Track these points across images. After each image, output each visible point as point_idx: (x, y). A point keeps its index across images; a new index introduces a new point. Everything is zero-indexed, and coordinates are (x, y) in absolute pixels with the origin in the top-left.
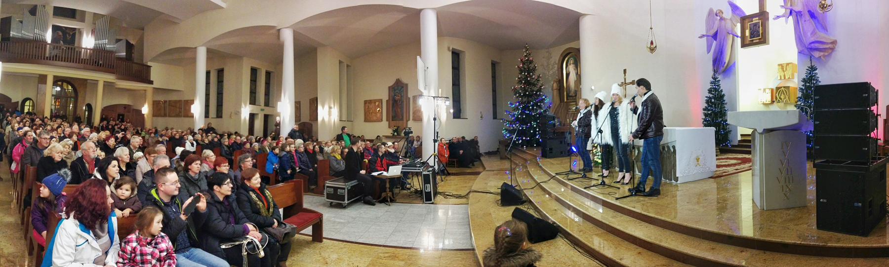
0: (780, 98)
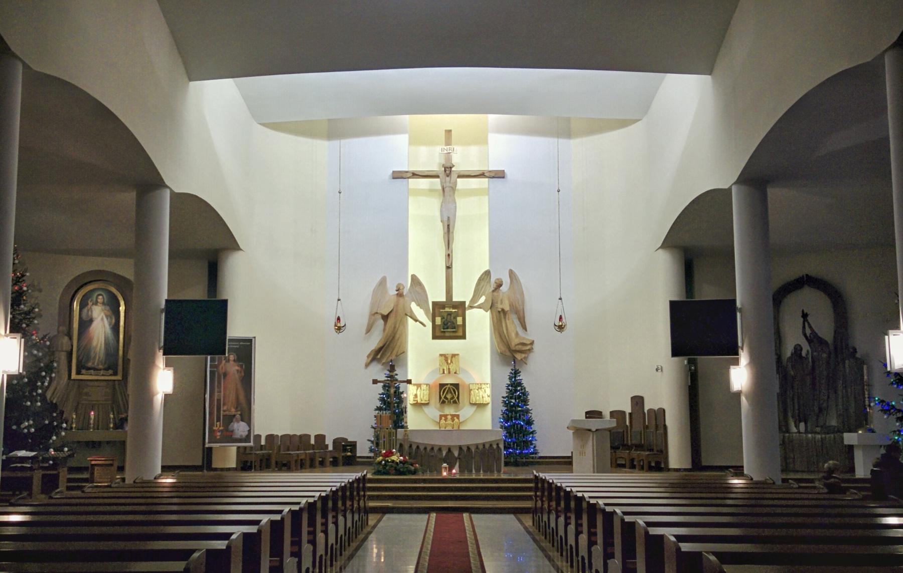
0: (445, 397)
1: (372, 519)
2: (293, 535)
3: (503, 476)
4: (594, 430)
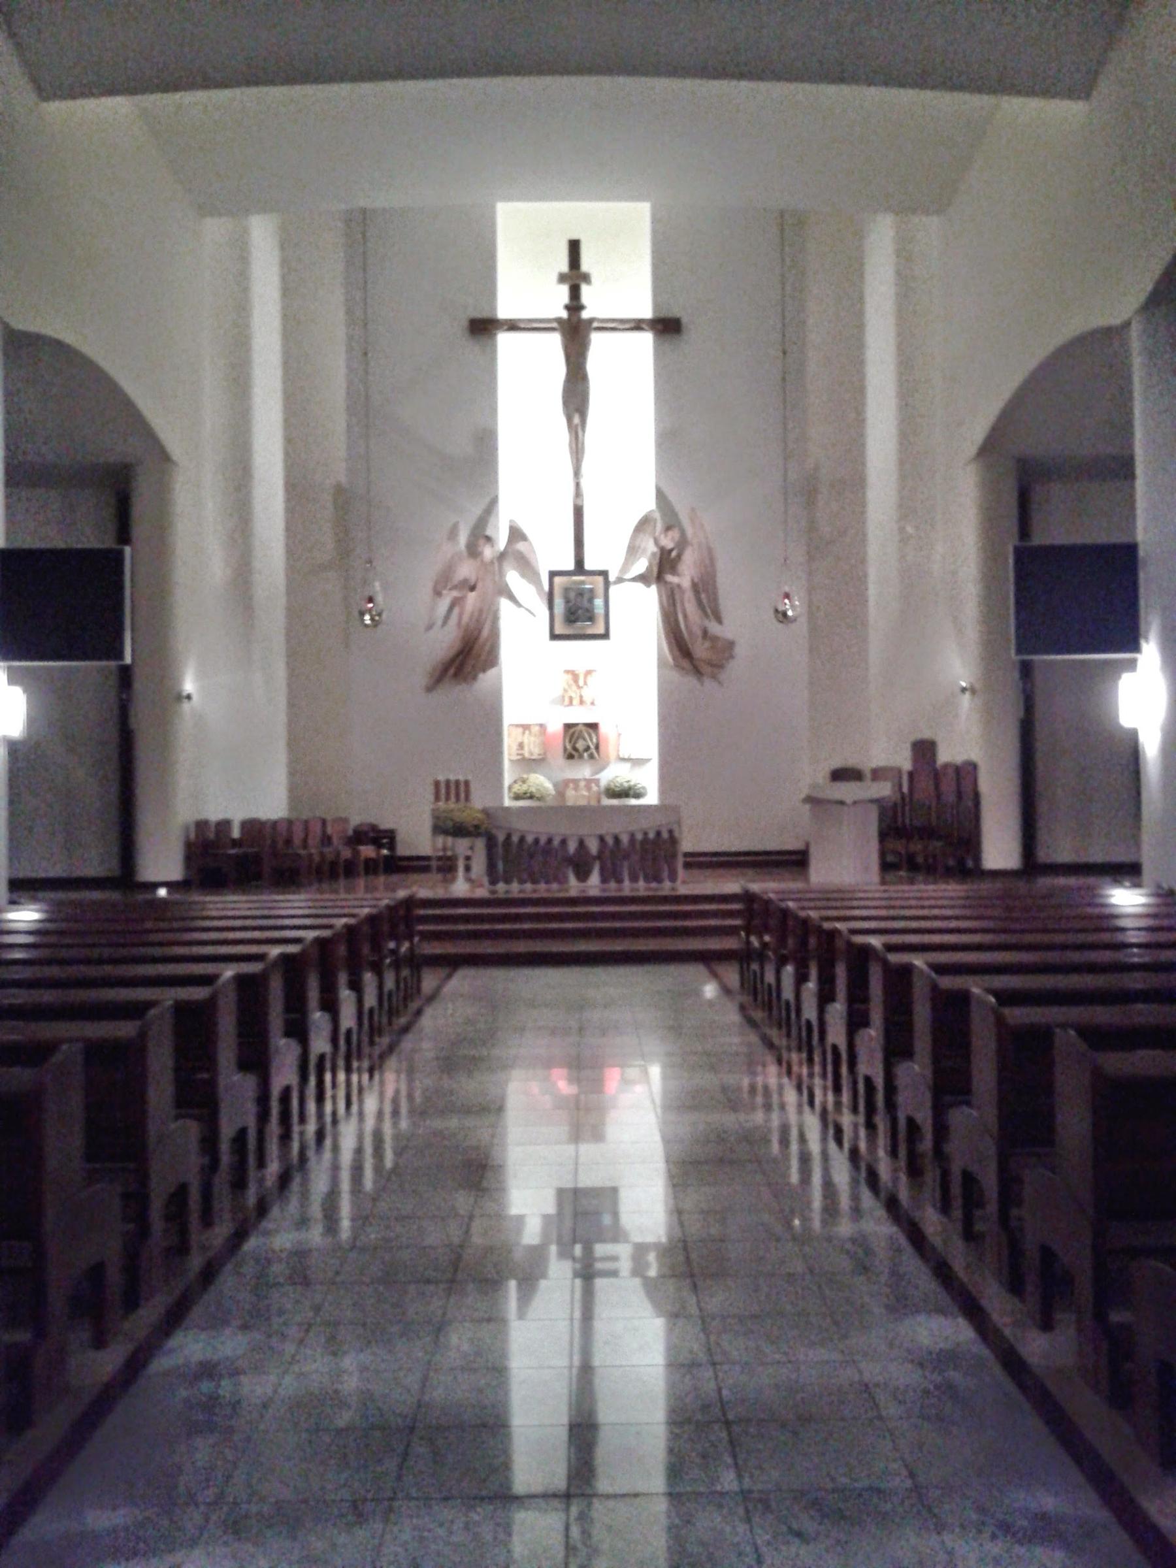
1: (429, 980)
2: (288, 1009)
3: (683, 890)
4: (849, 801)
